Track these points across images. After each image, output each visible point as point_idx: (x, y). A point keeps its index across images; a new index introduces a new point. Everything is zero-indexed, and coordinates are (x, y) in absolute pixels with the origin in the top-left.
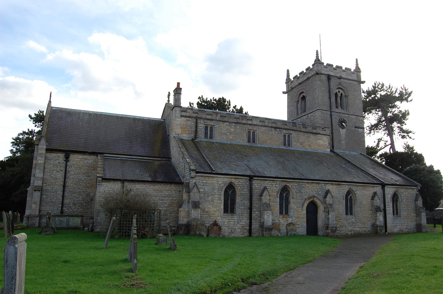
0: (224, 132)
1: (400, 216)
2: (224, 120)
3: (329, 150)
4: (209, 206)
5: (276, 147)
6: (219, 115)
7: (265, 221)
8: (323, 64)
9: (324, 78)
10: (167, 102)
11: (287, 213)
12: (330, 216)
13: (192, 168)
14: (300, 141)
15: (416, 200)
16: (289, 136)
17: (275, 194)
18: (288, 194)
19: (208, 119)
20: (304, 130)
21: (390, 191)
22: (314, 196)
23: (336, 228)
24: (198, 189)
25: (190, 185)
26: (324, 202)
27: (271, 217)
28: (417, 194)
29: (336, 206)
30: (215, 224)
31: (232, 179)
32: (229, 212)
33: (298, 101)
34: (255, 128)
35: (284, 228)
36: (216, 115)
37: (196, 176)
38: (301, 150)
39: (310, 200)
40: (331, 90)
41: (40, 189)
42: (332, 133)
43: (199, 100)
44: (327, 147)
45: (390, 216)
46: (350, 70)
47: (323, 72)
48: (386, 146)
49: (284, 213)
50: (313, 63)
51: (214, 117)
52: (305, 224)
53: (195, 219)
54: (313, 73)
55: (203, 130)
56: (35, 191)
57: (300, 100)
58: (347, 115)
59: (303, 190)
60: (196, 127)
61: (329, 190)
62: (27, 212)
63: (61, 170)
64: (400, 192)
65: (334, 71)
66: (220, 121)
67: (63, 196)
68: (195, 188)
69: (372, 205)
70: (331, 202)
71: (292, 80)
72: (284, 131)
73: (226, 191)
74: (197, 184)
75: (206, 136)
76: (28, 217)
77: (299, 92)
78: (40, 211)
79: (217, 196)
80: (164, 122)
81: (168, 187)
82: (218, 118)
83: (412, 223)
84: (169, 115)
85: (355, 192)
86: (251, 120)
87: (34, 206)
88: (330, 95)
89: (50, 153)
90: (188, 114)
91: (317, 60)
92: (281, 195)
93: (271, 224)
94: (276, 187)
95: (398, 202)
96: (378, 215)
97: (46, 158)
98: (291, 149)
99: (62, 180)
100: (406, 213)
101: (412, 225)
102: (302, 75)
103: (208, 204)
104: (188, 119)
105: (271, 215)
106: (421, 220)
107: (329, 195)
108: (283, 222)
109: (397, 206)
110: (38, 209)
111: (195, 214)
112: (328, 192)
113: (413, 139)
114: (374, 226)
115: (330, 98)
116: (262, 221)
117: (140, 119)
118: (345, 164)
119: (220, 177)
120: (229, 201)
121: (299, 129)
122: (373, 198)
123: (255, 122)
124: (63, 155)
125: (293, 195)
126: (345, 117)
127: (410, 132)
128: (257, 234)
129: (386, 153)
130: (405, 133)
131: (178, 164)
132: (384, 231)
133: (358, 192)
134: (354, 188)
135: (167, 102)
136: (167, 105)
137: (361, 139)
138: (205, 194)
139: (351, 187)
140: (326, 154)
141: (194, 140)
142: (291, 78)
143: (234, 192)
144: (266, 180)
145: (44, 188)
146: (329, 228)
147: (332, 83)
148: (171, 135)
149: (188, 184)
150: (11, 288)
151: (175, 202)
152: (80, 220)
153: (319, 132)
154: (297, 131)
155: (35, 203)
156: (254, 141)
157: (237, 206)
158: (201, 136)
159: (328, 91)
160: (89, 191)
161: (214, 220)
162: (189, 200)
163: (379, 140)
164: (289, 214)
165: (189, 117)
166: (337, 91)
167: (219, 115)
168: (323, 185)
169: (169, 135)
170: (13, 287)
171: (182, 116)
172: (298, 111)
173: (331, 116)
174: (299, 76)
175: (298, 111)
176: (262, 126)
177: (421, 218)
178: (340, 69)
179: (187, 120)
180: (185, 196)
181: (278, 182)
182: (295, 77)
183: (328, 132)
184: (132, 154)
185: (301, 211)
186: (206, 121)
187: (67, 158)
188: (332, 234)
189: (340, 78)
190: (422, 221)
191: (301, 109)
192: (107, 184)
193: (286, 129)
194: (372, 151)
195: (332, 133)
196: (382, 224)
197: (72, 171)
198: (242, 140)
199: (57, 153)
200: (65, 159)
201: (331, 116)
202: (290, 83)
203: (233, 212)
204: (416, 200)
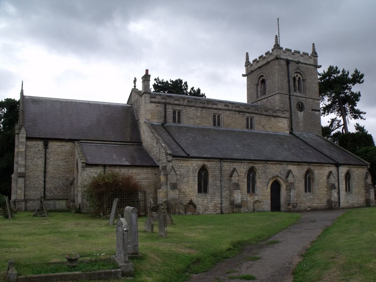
0: (191, 116)
1: (352, 193)
2: (191, 105)
3: (288, 132)
4: (185, 187)
5: (240, 130)
6: (186, 100)
7: (235, 199)
8: (282, 49)
9: (283, 63)
10: (133, 88)
11: (253, 191)
12: (292, 193)
13: (169, 152)
14: (262, 124)
15: (366, 178)
16: (251, 120)
17: (243, 174)
18: (254, 174)
19: (176, 105)
20: (265, 113)
21: (343, 170)
22: (277, 176)
23: (297, 204)
24: (175, 172)
25: (167, 168)
26: (286, 182)
27: (240, 195)
28: (367, 173)
29: (296, 185)
30: (191, 203)
31: (205, 162)
32: (203, 192)
33: (258, 84)
34: (220, 112)
35: (251, 205)
36: (184, 100)
37: (172, 160)
38: (263, 132)
39: (274, 179)
40: (290, 74)
41: (22, 175)
42: (291, 116)
43: (155, 82)
44: (287, 130)
45: (343, 192)
46: (308, 54)
47: (282, 57)
48: (339, 126)
49: (251, 192)
50: (273, 48)
51: (181, 102)
52: (269, 202)
53: (174, 199)
54: (272, 58)
55: (172, 115)
56: (19, 177)
57: (260, 83)
58: (304, 99)
59: (268, 171)
60: (165, 112)
61: (290, 170)
62: (13, 197)
63: (41, 157)
64: (352, 171)
65: (293, 55)
66: (187, 106)
67: (45, 182)
68: (173, 171)
69: (328, 183)
70: (292, 181)
71: (252, 63)
72: (247, 115)
73: (199, 174)
74: (174, 167)
75: (174, 121)
76: (15, 202)
77: (259, 76)
78: (25, 196)
79: (191, 177)
80: (131, 107)
81: (145, 170)
82: (185, 103)
83: (362, 198)
84: (137, 101)
85: (314, 172)
86: (216, 104)
87: (19, 191)
88: (289, 79)
89: (30, 141)
90: (156, 100)
91: (276, 45)
92: (248, 175)
93: (240, 202)
94: (244, 168)
95: (350, 180)
96: (333, 192)
97: (26, 146)
98: (253, 131)
99: (43, 166)
100: (356, 190)
101: (361, 200)
102: (262, 59)
103: (184, 185)
104: (157, 104)
105: (240, 194)
106: (370, 196)
107: (291, 174)
108: (250, 199)
109: (349, 184)
110: (23, 194)
111: (173, 194)
112: (289, 172)
113: (365, 119)
114: (329, 202)
115: (289, 82)
116: (232, 199)
117: (109, 105)
118: (304, 145)
119: (304, 165)
120: (203, 182)
121: (260, 113)
122: (328, 177)
123: (220, 107)
124: (42, 142)
125: (259, 176)
126: (303, 100)
127: (361, 113)
128: (227, 211)
129: (339, 133)
130: (357, 114)
131: (152, 148)
132: (338, 206)
133: (316, 172)
134: (312, 168)
135: (133, 88)
136: (134, 91)
137: (318, 121)
138: (181, 176)
139: (206, 163)
140: (285, 136)
141: (164, 124)
142: (251, 61)
143: (207, 174)
144: (235, 162)
145: (27, 174)
146: (291, 205)
147: (290, 68)
148: (140, 120)
149: (165, 168)
150: (136, 239)
151: (152, 184)
152: (65, 202)
153: (279, 114)
154: (259, 114)
155: (20, 189)
156: (219, 125)
157: (209, 186)
158: (170, 121)
159: (287, 75)
160: (68, 175)
161: (190, 200)
162: (167, 182)
163: (333, 120)
164: (255, 192)
165: (159, 103)
166: (295, 75)
167: (186, 100)
168: (285, 165)
169: (137, 120)
170: (137, 238)
171: (151, 102)
172: (257, 94)
173: (290, 99)
174: (258, 59)
175: (257, 94)
176: (226, 110)
177: (369, 194)
178: (298, 54)
179: (157, 106)
180: (163, 178)
181: (246, 164)
182: (255, 61)
183: (287, 115)
184: (106, 140)
185: (266, 189)
186: (174, 106)
187: (46, 146)
188: (293, 209)
189: (298, 63)
190: (371, 197)
191: (261, 92)
192: (90, 169)
193: (249, 113)
194: (326, 131)
195: (291, 116)
196: (337, 200)
197: (51, 158)
198: (208, 124)
199: (37, 141)
200: (44, 146)
201: (290, 99)
202: (249, 66)
203: (206, 192)
204: (366, 178)
